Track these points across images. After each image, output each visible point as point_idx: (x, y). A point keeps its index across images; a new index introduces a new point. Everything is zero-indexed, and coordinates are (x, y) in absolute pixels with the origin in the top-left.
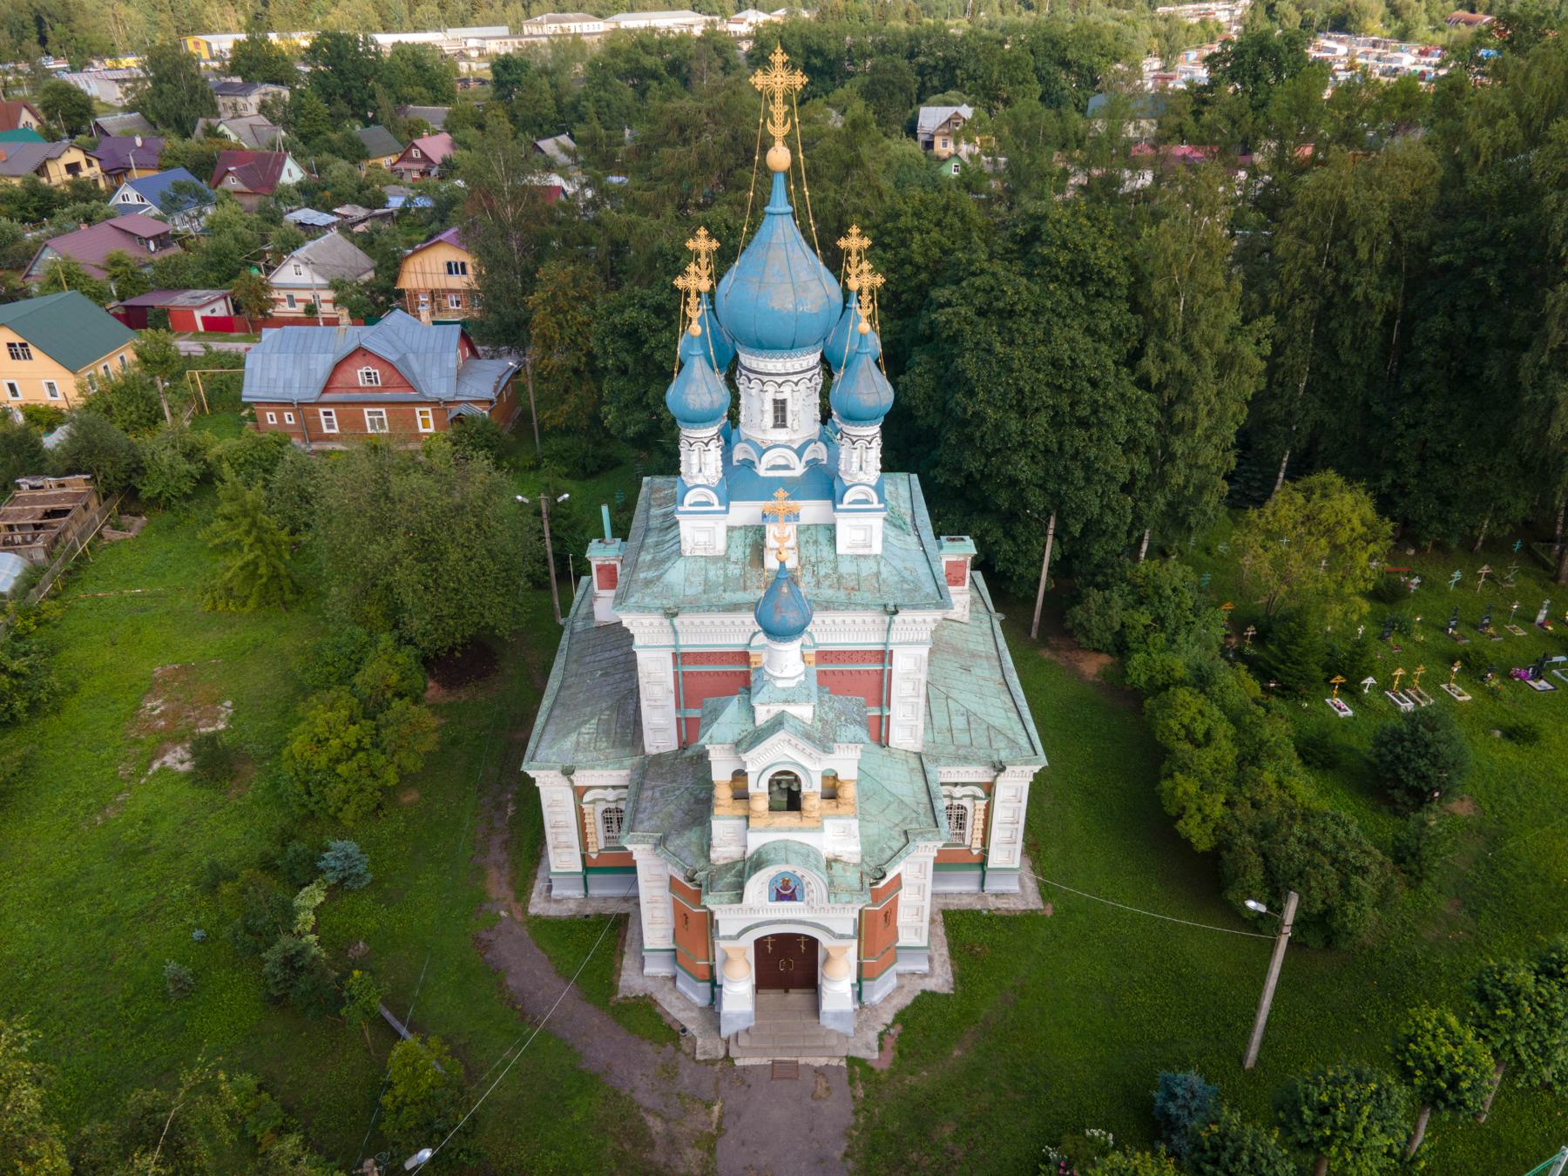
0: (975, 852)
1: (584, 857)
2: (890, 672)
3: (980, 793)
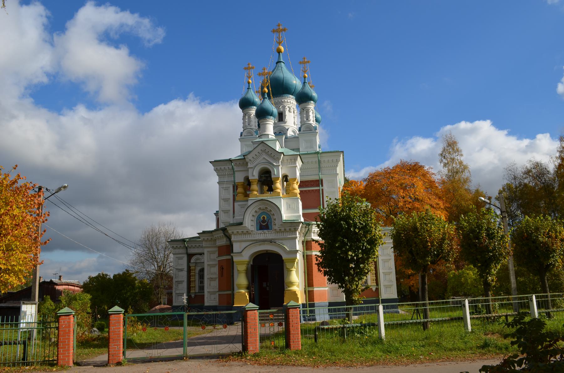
2: (322, 190)
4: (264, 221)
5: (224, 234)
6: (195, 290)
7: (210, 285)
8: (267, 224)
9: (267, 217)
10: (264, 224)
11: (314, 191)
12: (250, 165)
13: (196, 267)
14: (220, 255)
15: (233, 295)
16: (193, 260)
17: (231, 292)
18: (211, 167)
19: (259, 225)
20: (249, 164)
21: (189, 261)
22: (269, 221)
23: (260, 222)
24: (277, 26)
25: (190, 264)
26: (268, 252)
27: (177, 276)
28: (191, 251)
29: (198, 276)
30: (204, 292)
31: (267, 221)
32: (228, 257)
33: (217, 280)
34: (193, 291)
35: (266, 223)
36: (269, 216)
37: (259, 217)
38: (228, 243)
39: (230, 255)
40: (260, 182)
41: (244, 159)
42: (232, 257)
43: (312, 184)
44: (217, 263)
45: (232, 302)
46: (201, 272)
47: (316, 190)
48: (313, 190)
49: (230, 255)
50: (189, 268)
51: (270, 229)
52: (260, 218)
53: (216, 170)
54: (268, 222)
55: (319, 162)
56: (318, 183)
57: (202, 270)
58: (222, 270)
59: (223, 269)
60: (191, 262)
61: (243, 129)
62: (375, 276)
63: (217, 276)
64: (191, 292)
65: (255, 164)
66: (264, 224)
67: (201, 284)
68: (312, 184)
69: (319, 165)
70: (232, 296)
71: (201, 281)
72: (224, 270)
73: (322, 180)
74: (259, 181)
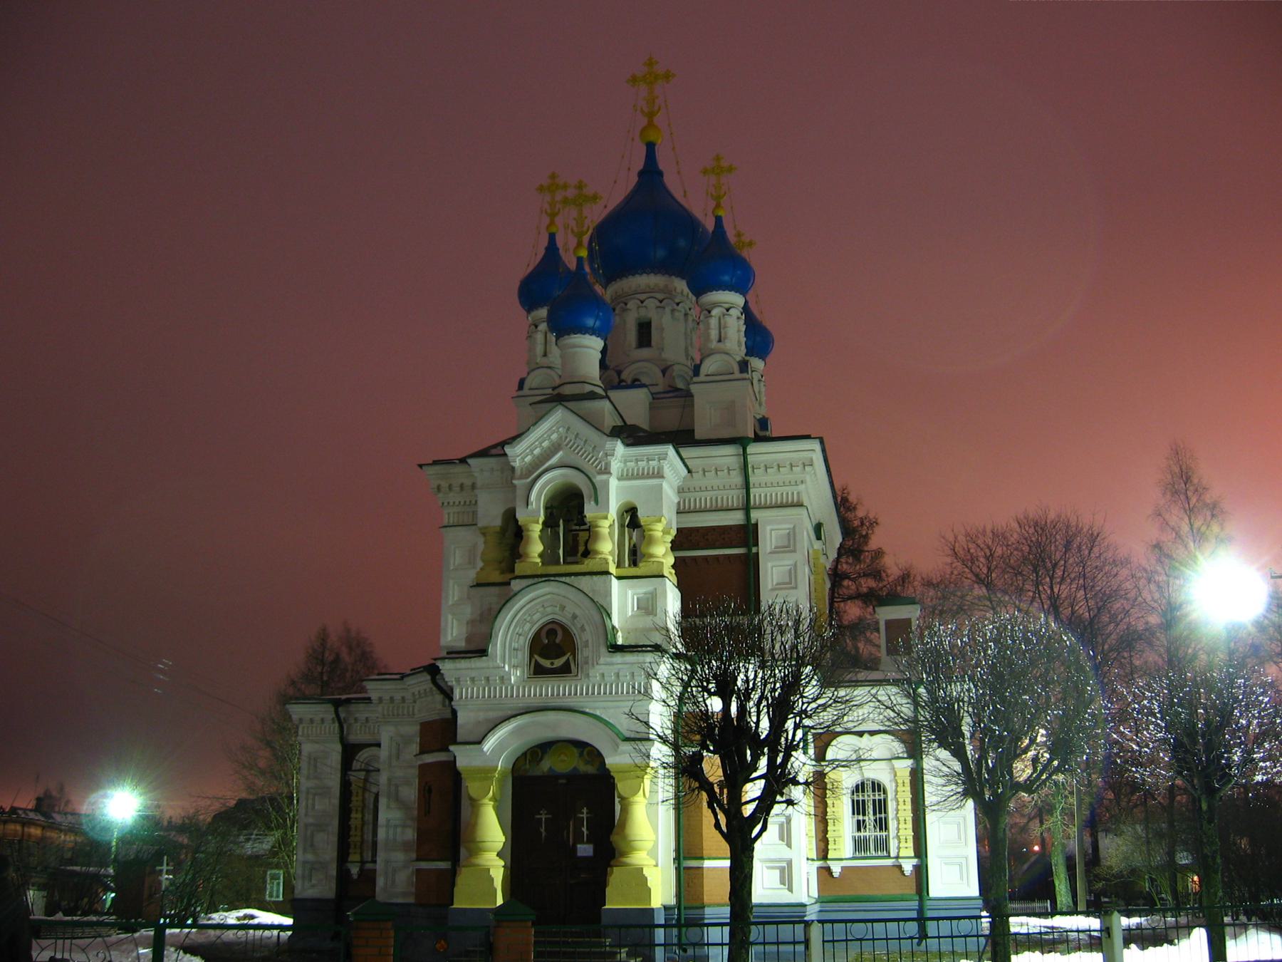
0: (908, 866)
28: (356, 736)
46: (857, 791)
59: (430, 791)
64: (351, 858)
67: (859, 829)
71: (858, 821)
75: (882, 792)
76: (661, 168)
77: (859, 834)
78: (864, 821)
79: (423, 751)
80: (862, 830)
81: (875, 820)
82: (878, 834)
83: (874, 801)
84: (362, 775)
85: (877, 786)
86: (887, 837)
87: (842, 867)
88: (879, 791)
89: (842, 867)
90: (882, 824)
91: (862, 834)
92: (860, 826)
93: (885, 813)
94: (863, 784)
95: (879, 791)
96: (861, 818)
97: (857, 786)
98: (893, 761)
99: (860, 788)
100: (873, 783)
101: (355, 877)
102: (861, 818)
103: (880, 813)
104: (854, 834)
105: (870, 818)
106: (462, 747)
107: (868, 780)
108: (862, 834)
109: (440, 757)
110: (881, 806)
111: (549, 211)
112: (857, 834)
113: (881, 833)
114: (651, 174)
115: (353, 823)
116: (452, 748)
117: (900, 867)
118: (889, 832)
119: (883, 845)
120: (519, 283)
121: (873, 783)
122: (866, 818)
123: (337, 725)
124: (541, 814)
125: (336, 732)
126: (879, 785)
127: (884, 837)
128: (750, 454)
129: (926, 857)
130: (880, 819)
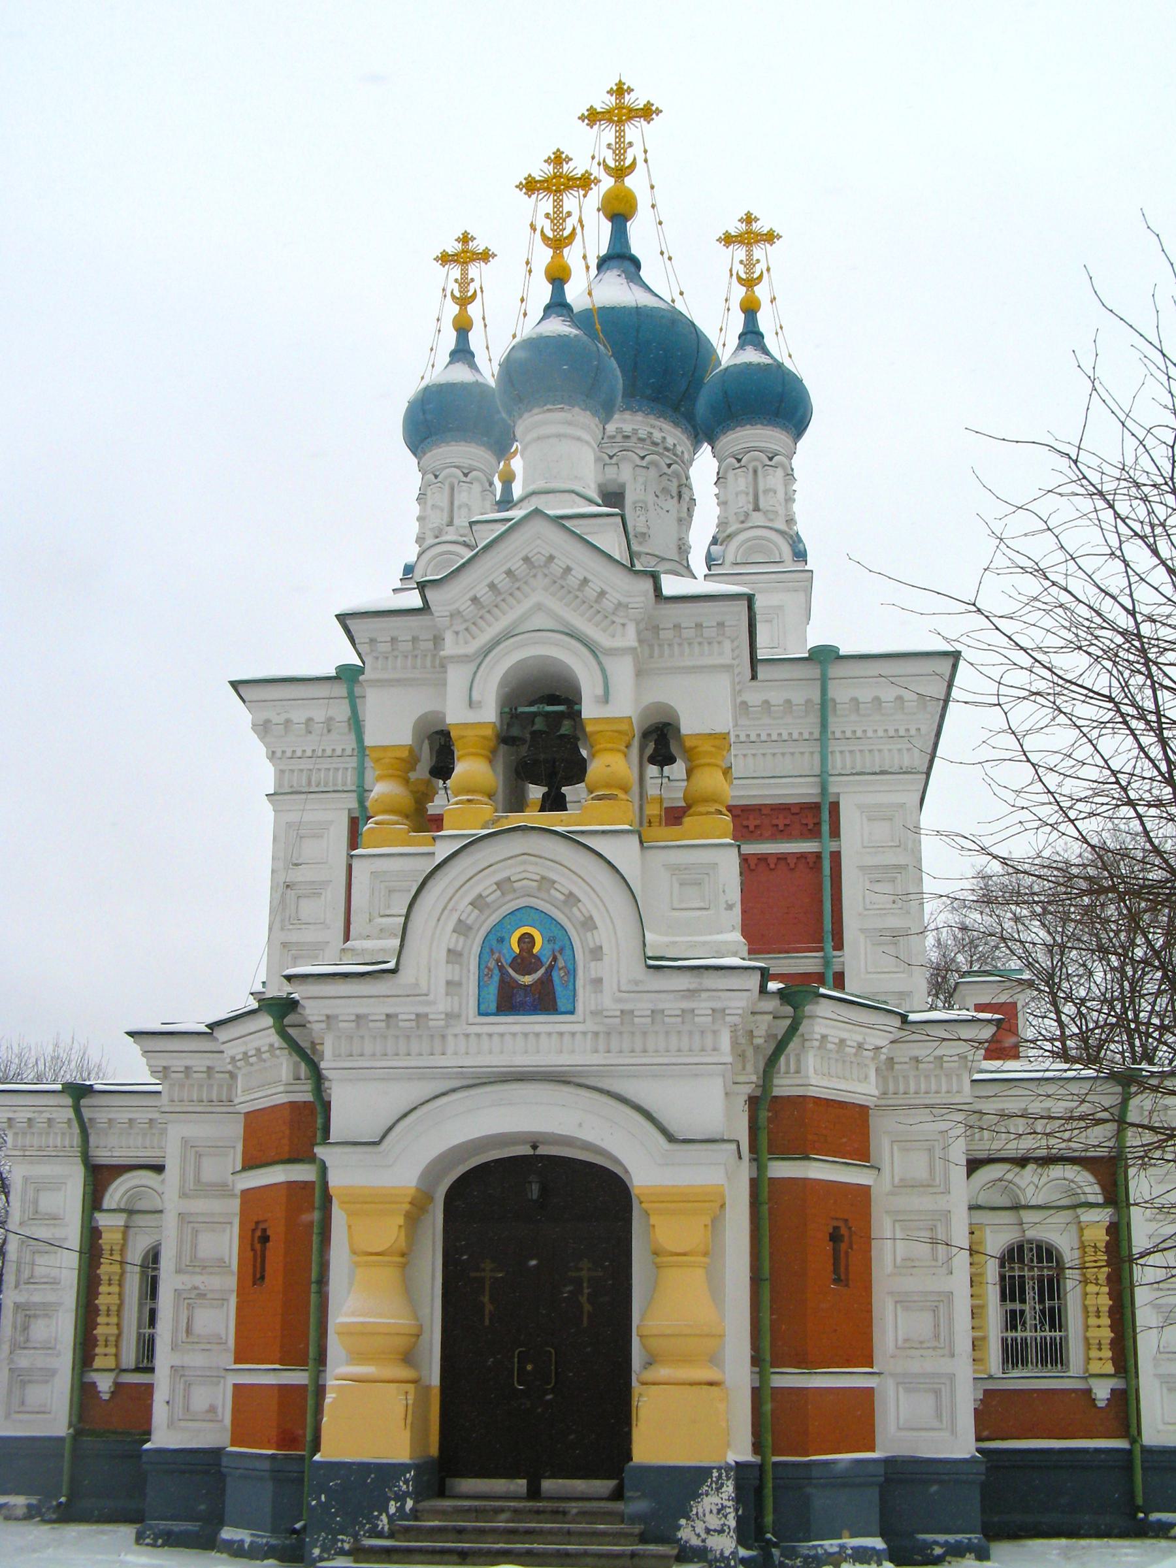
0: (1102, 1392)
1: (84, 1392)
2: (836, 857)
3: (1088, 1185)
4: (526, 960)
5: (283, 1033)
6: (117, 1355)
7: (189, 1331)
8: (547, 981)
9: (551, 940)
10: (528, 980)
11: (792, 862)
12: (450, 647)
13: (132, 1231)
14: (251, 1163)
15: (320, 1391)
16: (115, 1194)
17: (305, 1374)
18: (241, 715)
19: (496, 978)
20: (449, 637)
21: (94, 1201)
22: (561, 963)
23: (501, 968)
24: (610, 92)
25: (98, 1215)
26: (542, 1150)
27: (26, 1274)
28: (108, 1151)
29: (137, 1278)
30: (151, 1370)
31: (547, 960)
32: (303, 1173)
33: (233, 1300)
34: (110, 1363)
35: (542, 971)
36: (561, 943)
37: (497, 936)
38: (305, 1095)
39: (311, 1158)
40: (503, 748)
41: (426, 609)
42: (323, 1170)
43: (781, 822)
44: (235, 1205)
45: (309, 1437)
47: (802, 856)
48: (782, 858)
49: (311, 1158)
50: (92, 1236)
51: (561, 1007)
52: (501, 940)
53: (263, 729)
54: (551, 968)
55: (825, 708)
56: (810, 822)
57: (153, 1257)
58: (258, 1246)
59: (265, 1239)
60: (105, 1206)
61: (416, 549)
62: (1108, 1322)
63: (232, 1282)
64: (98, 1363)
65: (484, 638)
66: (528, 980)
68: (781, 822)
69: (824, 725)
70: (311, 1402)
72: (269, 1245)
73: (835, 807)
74: (506, 739)
75: (1055, 1264)
76: (472, 348)
77: (1014, 1334)
78: (1022, 1312)
79: (251, 1163)
80: (1019, 1328)
81: (1043, 1311)
82: (1048, 1334)
83: (1041, 1279)
84: (120, 1220)
85: (1046, 1253)
86: (1064, 1340)
87: (986, 1391)
88: (1050, 1260)
89: (986, 1391)
90: (1054, 1318)
91: (1019, 1334)
92: (1013, 1320)
93: (1059, 1298)
94: (1021, 1248)
95: (1050, 1260)
96: (1017, 1306)
97: (1011, 1251)
98: (1080, 1211)
99: (1013, 1255)
100: (1039, 1248)
101: (106, 1397)
102: (1017, 1306)
103: (1051, 1298)
104: (1005, 1335)
105: (1030, 1307)
106: (338, 1150)
107: (1030, 1242)
108: (1019, 1334)
109: (303, 1173)
110: (1051, 1288)
111: (457, 294)
112: (1010, 1334)
113: (1053, 1334)
114: (450, 363)
115: (102, 1301)
116: (319, 1151)
117: (1089, 1391)
118: (1066, 1330)
119: (1053, 1354)
120: (407, 404)
121: (1039, 1248)
122: (1027, 1307)
123: (76, 1130)
124: (484, 1270)
125: (75, 1144)
126: (1049, 1253)
127: (1058, 1341)
128: (270, 1027)
129: (1137, 1377)
130: (1052, 1309)
